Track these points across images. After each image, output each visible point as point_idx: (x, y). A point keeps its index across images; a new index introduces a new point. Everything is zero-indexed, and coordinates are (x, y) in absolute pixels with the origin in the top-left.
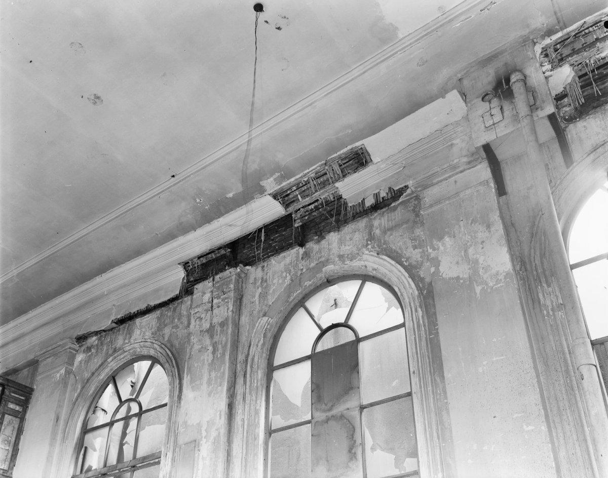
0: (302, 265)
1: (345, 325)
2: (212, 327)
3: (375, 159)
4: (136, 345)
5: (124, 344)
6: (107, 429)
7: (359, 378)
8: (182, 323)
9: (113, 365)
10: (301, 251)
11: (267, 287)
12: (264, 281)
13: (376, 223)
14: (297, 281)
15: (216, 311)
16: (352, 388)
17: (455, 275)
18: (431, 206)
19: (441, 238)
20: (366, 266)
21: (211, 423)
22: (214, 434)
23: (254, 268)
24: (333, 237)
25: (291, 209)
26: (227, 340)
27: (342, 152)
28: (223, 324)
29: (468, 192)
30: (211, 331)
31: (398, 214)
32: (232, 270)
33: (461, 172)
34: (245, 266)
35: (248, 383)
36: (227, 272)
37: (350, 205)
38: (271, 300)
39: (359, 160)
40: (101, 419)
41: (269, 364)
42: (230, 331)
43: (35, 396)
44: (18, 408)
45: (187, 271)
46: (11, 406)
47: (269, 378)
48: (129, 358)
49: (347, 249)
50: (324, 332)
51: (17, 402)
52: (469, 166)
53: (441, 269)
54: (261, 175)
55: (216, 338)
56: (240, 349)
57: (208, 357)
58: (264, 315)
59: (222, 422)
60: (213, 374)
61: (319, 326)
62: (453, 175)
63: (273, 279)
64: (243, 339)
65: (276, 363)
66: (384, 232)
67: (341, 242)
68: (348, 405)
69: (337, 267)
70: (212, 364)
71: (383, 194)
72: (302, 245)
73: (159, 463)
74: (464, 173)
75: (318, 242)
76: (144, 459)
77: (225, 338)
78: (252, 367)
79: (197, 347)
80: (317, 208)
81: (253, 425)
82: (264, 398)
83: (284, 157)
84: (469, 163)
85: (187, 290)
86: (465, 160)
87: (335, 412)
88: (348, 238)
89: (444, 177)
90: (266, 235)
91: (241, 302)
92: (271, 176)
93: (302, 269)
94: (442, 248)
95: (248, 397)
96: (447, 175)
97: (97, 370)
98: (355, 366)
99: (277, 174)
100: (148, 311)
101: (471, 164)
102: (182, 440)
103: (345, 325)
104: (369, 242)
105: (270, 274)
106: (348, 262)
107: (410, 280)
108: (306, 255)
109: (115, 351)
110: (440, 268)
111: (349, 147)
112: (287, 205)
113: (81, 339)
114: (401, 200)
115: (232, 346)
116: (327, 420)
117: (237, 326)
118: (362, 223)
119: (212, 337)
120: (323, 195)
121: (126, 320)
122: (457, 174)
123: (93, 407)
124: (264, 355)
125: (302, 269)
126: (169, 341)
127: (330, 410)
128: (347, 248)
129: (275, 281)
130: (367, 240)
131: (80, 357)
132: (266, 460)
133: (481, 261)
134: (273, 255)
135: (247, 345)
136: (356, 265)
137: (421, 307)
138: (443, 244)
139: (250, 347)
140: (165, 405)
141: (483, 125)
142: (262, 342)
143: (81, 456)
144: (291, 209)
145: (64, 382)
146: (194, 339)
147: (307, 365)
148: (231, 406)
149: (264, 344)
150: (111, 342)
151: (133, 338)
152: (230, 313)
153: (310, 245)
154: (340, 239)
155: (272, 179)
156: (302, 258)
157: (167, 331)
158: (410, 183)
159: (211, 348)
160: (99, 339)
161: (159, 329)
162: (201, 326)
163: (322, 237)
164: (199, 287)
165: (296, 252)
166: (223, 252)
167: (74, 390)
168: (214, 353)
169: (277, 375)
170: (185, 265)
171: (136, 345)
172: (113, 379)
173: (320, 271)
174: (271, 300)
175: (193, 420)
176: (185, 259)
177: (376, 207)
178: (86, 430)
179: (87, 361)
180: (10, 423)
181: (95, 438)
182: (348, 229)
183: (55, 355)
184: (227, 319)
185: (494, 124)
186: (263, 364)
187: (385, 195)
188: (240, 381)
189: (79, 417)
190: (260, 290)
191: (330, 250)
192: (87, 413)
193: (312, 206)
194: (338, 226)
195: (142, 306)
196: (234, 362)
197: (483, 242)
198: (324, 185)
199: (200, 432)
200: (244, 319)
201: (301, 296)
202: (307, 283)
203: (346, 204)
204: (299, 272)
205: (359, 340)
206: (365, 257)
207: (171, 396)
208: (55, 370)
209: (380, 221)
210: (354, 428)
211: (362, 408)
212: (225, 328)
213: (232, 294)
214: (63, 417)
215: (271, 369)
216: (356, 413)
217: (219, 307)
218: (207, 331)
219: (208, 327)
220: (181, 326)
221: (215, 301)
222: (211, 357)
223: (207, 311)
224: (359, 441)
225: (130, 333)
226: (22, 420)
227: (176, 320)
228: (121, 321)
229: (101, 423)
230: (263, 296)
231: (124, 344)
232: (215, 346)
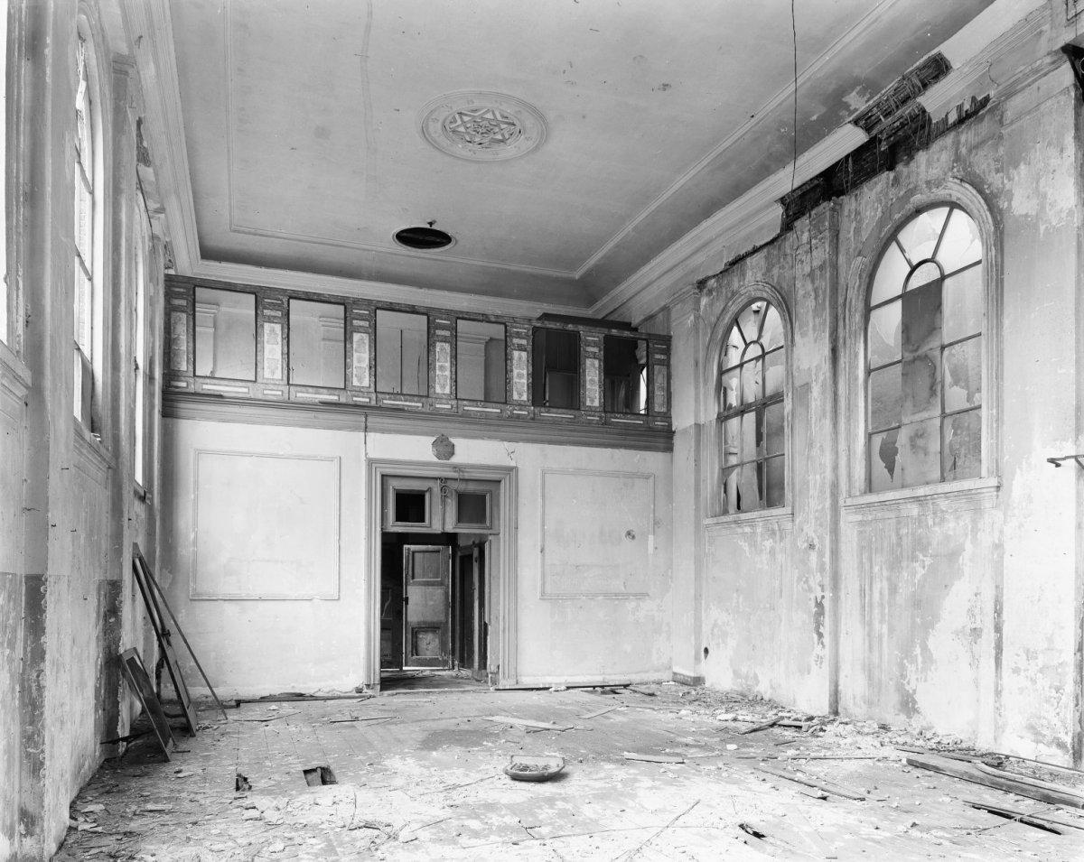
0: (892, 193)
1: (932, 260)
2: (812, 271)
3: (955, 64)
4: (751, 289)
5: (740, 287)
6: (738, 370)
7: (941, 319)
8: (788, 263)
9: (734, 309)
10: (892, 175)
11: (860, 222)
12: (858, 213)
13: (963, 138)
14: (887, 214)
15: (814, 253)
16: (935, 329)
17: (1024, 213)
18: (1012, 123)
19: (1016, 167)
20: (951, 195)
21: (818, 368)
22: (822, 378)
23: (848, 197)
24: (921, 157)
25: (874, 132)
26: (826, 285)
27: (918, 63)
28: (822, 268)
29: (1049, 103)
30: (811, 275)
31: (984, 127)
32: (825, 204)
33: (1045, 75)
34: (838, 197)
35: (848, 327)
36: (821, 207)
37: (934, 122)
38: (864, 236)
39: (939, 68)
40: (734, 358)
41: (866, 304)
42: (828, 275)
43: (674, 343)
44: (663, 357)
45: (784, 205)
46: (658, 356)
47: (866, 319)
48: (746, 300)
49: (935, 172)
50: (914, 269)
51: (662, 352)
52: (1053, 67)
53: (1014, 204)
54: (842, 91)
55: (817, 283)
56: (840, 291)
57: (811, 303)
58: (859, 255)
59: (827, 367)
60: (817, 321)
61: (909, 262)
62: (1035, 80)
63: (866, 211)
64: (842, 281)
65: (873, 303)
66: (970, 151)
67: (929, 163)
68: (931, 346)
69: (924, 196)
70: (815, 310)
71: (967, 107)
72: (891, 168)
73: (783, 401)
74: (1048, 76)
75: (907, 164)
76: (771, 397)
77: (824, 284)
78: (850, 311)
79: (801, 292)
80: (903, 125)
81: (853, 367)
82: (862, 341)
83: (863, 70)
84: (1053, 63)
85: (787, 226)
86: (1048, 60)
87: (920, 352)
88: (936, 157)
89: (1026, 83)
90: (854, 162)
91: (837, 239)
92: (853, 90)
93: (892, 199)
94: (1016, 178)
95: (848, 341)
96: (1030, 80)
97: (720, 315)
98: (938, 307)
99: (858, 88)
100: (756, 250)
101: (1055, 65)
102: (797, 384)
103: (932, 260)
104: (955, 165)
105: (863, 205)
106: (934, 190)
107: (988, 213)
108: (896, 181)
109: (733, 294)
110: (1013, 202)
111: (925, 57)
112: (868, 129)
113: (701, 284)
114: (988, 107)
115: (831, 291)
116: (914, 360)
117: (835, 267)
118: (949, 140)
119: (813, 282)
120: (906, 111)
121: (739, 260)
122: (1040, 77)
123: (724, 347)
124: (861, 297)
125: (892, 199)
126: (778, 283)
127: (916, 350)
128: (935, 171)
129: (868, 213)
130: (954, 162)
131: (704, 301)
132: (866, 397)
133: (1049, 193)
134: (865, 180)
135: (845, 287)
136: (941, 193)
137: (995, 246)
138: (1019, 173)
139: (847, 290)
140: (782, 347)
141: (1065, 17)
142: (857, 284)
143: (722, 395)
144: (874, 132)
145: (696, 326)
146: (798, 284)
147: (898, 305)
148: (834, 351)
149: (860, 286)
150: (728, 284)
151: (747, 280)
152: (827, 256)
153: (900, 167)
154: (928, 160)
155: (854, 93)
156: (892, 185)
157: (775, 271)
158: (992, 93)
159: (813, 294)
160: (717, 281)
161: (769, 270)
162: (803, 270)
163: (911, 158)
164: (798, 224)
165: (886, 176)
166: (816, 182)
167: (705, 334)
168: (816, 299)
169: (874, 314)
170: (782, 200)
171: (751, 289)
172: (736, 321)
173: (908, 201)
174: (864, 236)
175: (805, 365)
176: (781, 196)
177: (961, 121)
178: (722, 372)
179: (711, 304)
180: (659, 372)
181: (731, 378)
182: (935, 147)
183: (682, 301)
184: (824, 262)
185: (1076, 15)
186: (861, 305)
187: (968, 107)
188: (841, 323)
189: (713, 362)
190: (854, 225)
191: (918, 174)
192: (720, 354)
193: (898, 123)
194: (926, 145)
195: (749, 248)
196: (834, 306)
197: (1054, 171)
198: (904, 101)
199: (810, 375)
200: (842, 259)
201: (893, 229)
202: (897, 216)
203: (930, 120)
204: (890, 203)
205: (943, 278)
206: (950, 184)
207: (786, 340)
208: (684, 318)
209: (967, 136)
210: (935, 367)
211: (943, 348)
212: (823, 272)
213: (827, 234)
214: (701, 361)
215: (868, 310)
216: (937, 353)
217: (816, 248)
218: (809, 275)
219: (809, 269)
220: (787, 266)
221: (814, 241)
222: (814, 303)
223: (806, 252)
224: (939, 379)
225: (743, 275)
226: (668, 365)
227: (782, 260)
228: (733, 263)
229: (733, 365)
230: (858, 231)
231: (740, 287)
232: (816, 290)
